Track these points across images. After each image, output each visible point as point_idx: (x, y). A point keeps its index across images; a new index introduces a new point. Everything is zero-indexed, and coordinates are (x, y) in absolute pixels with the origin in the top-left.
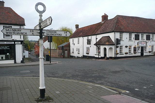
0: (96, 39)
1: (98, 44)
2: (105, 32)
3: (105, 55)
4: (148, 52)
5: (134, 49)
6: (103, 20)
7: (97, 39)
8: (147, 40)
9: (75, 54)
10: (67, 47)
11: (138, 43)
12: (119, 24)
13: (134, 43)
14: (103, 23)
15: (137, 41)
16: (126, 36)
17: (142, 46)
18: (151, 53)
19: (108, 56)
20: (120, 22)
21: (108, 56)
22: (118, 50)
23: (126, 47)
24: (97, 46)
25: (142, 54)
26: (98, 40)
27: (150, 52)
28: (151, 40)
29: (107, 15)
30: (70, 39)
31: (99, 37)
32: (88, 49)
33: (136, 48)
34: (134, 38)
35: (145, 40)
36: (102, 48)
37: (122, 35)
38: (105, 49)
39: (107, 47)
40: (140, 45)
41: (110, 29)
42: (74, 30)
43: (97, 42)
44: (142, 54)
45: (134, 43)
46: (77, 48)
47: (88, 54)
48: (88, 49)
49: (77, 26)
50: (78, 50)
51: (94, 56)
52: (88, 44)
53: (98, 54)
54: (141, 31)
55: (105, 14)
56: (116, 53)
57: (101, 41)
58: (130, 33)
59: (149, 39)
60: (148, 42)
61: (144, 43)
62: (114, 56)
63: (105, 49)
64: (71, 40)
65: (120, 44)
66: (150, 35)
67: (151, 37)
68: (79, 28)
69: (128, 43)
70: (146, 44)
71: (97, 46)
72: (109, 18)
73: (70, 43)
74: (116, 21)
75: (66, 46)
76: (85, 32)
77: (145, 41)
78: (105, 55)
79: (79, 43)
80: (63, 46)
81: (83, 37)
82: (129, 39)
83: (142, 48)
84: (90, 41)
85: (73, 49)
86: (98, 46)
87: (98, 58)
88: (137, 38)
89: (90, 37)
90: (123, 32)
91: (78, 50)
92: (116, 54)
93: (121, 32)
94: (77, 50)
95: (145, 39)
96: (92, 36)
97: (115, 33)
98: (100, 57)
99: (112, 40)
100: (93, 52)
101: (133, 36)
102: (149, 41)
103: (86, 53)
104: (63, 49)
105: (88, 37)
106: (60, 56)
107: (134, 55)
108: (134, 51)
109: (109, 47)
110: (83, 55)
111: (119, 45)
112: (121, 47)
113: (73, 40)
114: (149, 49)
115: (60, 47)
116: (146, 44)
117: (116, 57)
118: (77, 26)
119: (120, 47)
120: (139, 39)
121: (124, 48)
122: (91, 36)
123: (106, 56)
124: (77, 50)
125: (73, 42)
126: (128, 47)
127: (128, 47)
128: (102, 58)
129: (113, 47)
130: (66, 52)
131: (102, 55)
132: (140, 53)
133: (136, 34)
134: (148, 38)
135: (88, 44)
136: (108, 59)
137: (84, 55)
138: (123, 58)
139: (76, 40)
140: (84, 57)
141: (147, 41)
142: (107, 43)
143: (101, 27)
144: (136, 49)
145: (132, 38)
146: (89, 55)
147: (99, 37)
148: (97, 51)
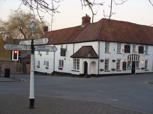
1: (76, 56)
5: (123, 65)
8: (139, 53)
11: (128, 56)
14: (84, 28)
15: (127, 54)
18: (145, 69)
19: (89, 73)
21: (89, 73)
23: (114, 61)
25: (133, 71)
27: (143, 69)
28: (144, 54)
31: (78, 46)
32: (61, 63)
34: (123, 50)
35: (137, 53)
36: (82, 61)
38: (86, 64)
39: (89, 61)
43: (74, 53)
44: (133, 71)
45: (124, 57)
46: (45, 60)
47: (62, 69)
48: (61, 63)
52: (61, 55)
55: (86, 15)
58: (119, 42)
60: (140, 55)
63: (86, 64)
67: (145, 49)
82: (80, 64)
83: (134, 63)
88: (127, 50)
89: (64, 46)
90: (110, 42)
94: (45, 63)
95: (138, 52)
99: (95, 52)
101: (123, 46)
105: (62, 46)
107: (123, 72)
120: (129, 52)
122: (66, 45)
123: (87, 73)
124: (45, 63)
128: (81, 76)
131: (81, 71)
133: (126, 44)
134: (141, 51)
135: (61, 55)
136: (89, 76)
137: (55, 70)
140: (55, 73)
141: (140, 54)
144: (126, 65)
145: (121, 52)
146: (63, 71)
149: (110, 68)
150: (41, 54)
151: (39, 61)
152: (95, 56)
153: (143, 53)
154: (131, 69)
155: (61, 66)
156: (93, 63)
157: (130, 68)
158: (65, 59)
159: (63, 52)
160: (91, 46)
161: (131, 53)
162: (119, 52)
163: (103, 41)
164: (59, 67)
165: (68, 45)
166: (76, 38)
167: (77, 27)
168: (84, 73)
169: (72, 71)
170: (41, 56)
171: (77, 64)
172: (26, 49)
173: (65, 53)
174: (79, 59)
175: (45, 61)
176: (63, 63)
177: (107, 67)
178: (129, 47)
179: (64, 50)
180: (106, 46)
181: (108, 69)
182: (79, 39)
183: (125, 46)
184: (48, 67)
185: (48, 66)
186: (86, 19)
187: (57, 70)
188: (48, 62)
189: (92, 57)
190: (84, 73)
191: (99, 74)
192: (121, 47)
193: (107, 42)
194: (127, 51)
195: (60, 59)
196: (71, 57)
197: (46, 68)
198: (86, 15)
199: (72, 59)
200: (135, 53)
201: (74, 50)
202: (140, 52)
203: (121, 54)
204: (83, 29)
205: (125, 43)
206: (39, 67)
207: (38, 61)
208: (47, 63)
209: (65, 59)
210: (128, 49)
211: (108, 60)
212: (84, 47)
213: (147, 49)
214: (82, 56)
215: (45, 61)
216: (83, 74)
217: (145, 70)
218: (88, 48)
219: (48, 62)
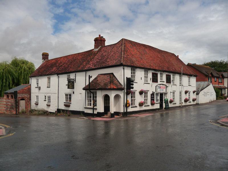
2: (104, 65)
3: (107, 108)
5: (151, 98)
6: (96, 46)
8: (167, 82)
9: (42, 106)
10: (25, 93)
11: (156, 87)
12: (128, 54)
13: (151, 88)
15: (155, 84)
16: (140, 74)
17: (162, 92)
18: (188, 102)
20: (129, 51)
26: (91, 80)
28: (172, 83)
30: (32, 78)
32: (69, 97)
33: (154, 96)
34: (151, 79)
35: (165, 83)
37: (135, 72)
39: (112, 95)
40: (159, 91)
41: (114, 61)
42: (38, 63)
43: (86, 85)
45: (151, 88)
47: (68, 106)
48: (69, 97)
49: (45, 56)
50: (47, 99)
52: (68, 88)
53: (92, 106)
54: (160, 69)
59: (169, 81)
60: (168, 86)
61: (164, 88)
62: (122, 111)
64: (33, 82)
66: (170, 76)
67: (172, 79)
68: (50, 58)
69: (145, 88)
72: (107, 43)
74: (123, 47)
75: (23, 92)
76: (61, 66)
77: (164, 85)
78: (107, 108)
79: (49, 85)
83: (50, 87)
84: (73, 83)
85: (37, 97)
87: (93, 115)
89: (72, 76)
91: (47, 99)
94: (45, 98)
97: (125, 68)
98: (95, 112)
99: (118, 81)
101: (150, 75)
102: (170, 85)
103: (65, 105)
104: (16, 97)
105: (69, 76)
106: (10, 110)
107: (151, 107)
112: (133, 93)
115: (10, 93)
117: (125, 111)
118: (45, 56)
120: (157, 81)
121: (137, 94)
124: (45, 98)
125: (38, 84)
128: (99, 115)
129: (122, 94)
130: (22, 103)
131: (100, 108)
132: (159, 104)
133: (154, 72)
134: (168, 80)
135: (68, 88)
137: (59, 108)
139: (43, 81)
141: (167, 85)
143: (93, 58)
144: (154, 98)
145: (149, 79)
146: (72, 108)
147: (94, 74)
150: (40, 87)
151: (38, 97)
152: (120, 87)
153: (170, 82)
155: (68, 102)
158: (74, 93)
159: (71, 84)
161: (159, 83)
162: (146, 83)
163: (128, 66)
164: (65, 104)
165: (77, 74)
167: (87, 51)
168: (104, 112)
170: (40, 89)
172: (49, 106)
173: (74, 84)
174: (96, 92)
175: (45, 97)
176: (70, 98)
178: (157, 74)
179: (72, 80)
182: (93, 65)
183: (153, 74)
184: (70, 102)
185: (50, 102)
186: (99, 41)
187: (62, 107)
188: (50, 97)
190: (104, 112)
193: (133, 68)
197: (45, 100)
198: (100, 35)
200: (163, 82)
201: (58, 97)
202: (168, 81)
204: (97, 53)
207: (37, 97)
208: (48, 99)
212: (101, 76)
213: (173, 78)
214: (100, 87)
215: (45, 97)
216: (103, 113)
217: (173, 104)
218: (108, 76)
219: (49, 97)
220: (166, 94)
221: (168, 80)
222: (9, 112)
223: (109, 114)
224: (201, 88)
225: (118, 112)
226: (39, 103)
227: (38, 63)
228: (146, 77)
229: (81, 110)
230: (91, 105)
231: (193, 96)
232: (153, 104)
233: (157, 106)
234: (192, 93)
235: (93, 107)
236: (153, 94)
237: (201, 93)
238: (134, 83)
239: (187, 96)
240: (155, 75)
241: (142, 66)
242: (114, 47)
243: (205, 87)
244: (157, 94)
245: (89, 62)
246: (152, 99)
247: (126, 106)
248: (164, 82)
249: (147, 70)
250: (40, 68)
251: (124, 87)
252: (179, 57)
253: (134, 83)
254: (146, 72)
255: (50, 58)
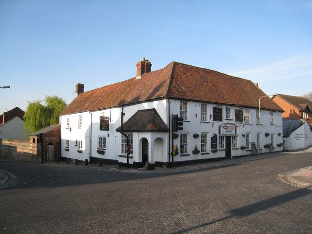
0: (123, 114)
1: (126, 129)
3: (145, 156)
4: (240, 148)
7: (124, 117)
11: (220, 127)
14: (140, 80)
15: (218, 124)
16: (193, 110)
18: (245, 150)
19: (151, 160)
21: (151, 160)
22: (177, 142)
23: (196, 136)
24: (125, 133)
25: (228, 152)
26: (126, 119)
27: (243, 148)
28: (244, 122)
29: (150, 63)
31: (131, 111)
32: (102, 141)
33: (216, 140)
35: (234, 122)
36: (137, 138)
38: (144, 142)
39: (148, 136)
42: (69, 96)
43: (124, 122)
44: (228, 152)
45: (211, 128)
47: (102, 153)
48: (102, 141)
50: (78, 145)
51: (117, 159)
52: (101, 129)
53: (126, 155)
55: (80, 88)
56: (171, 152)
57: (135, 121)
58: (204, 103)
63: (144, 142)
64: (63, 119)
65: (181, 129)
69: (200, 128)
70: (236, 130)
71: (125, 133)
73: (60, 126)
77: (232, 124)
78: (145, 156)
80: (44, 133)
81: (91, 111)
82: (133, 144)
86: (126, 135)
87: (127, 166)
88: (217, 116)
89: (106, 113)
90: (189, 100)
92: (173, 155)
93: (184, 100)
95: (234, 119)
96: (112, 109)
98: (131, 162)
100: (114, 150)
101: (210, 110)
107: (212, 156)
108: (212, 148)
109: (156, 138)
110: (91, 158)
111: (179, 133)
113: (68, 119)
114: (240, 142)
116: (236, 130)
117: (171, 161)
119: (202, 137)
120: (221, 120)
121: (190, 138)
122: (109, 110)
123: (147, 160)
124: (77, 143)
125: (68, 124)
126: (270, 136)
127: (200, 136)
128: (136, 165)
129: (165, 137)
130: (51, 148)
131: (137, 157)
133: (215, 106)
134: (239, 117)
135: (101, 129)
136: (152, 167)
137: (93, 156)
138: (272, 206)
139: (73, 118)
140: (93, 160)
141: (238, 124)
142: (150, 127)
144: (216, 142)
145: (208, 119)
148: (124, 147)
149: (190, 148)
150: (71, 128)
154: (223, 150)
156: (159, 140)
157: (222, 149)
158: (108, 135)
160: (154, 110)
162: (203, 120)
165: (113, 110)
166: (127, 97)
169: (119, 156)
170: (71, 131)
171: (128, 143)
174: (132, 135)
176: (105, 143)
177: (124, 149)
178: (221, 110)
180: (181, 109)
181: (186, 152)
183: (214, 109)
187: (96, 155)
189: (156, 129)
191: (174, 161)
192: (208, 110)
193: (183, 101)
194: (217, 118)
195: (100, 136)
196: (118, 130)
199: (119, 134)
203: (207, 124)
204: (139, 82)
205: (214, 103)
206: (68, 150)
209: (108, 135)
210: (216, 114)
211: (186, 135)
220: (235, 137)
221: (239, 117)
222: (35, 159)
223: (146, 165)
224: (292, 128)
225: (162, 162)
226: (69, 149)
227: (69, 96)
228: (204, 113)
229: (114, 159)
230: (223, 147)
231: (278, 140)
232: (214, 151)
233: (222, 154)
234: (275, 136)
235: (128, 155)
236: (214, 138)
237: (293, 134)
238: (183, 122)
239: (268, 141)
240: (217, 111)
241: (196, 99)
242: (160, 74)
243: (297, 126)
244: (222, 138)
245: (128, 94)
246: (214, 145)
247: (173, 153)
248: (232, 120)
249: (205, 104)
250: (72, 104)
251: (169, 128)
252: (260, 87)
253: (183, 122)
254: (184, 105)
255: (85, 90)
